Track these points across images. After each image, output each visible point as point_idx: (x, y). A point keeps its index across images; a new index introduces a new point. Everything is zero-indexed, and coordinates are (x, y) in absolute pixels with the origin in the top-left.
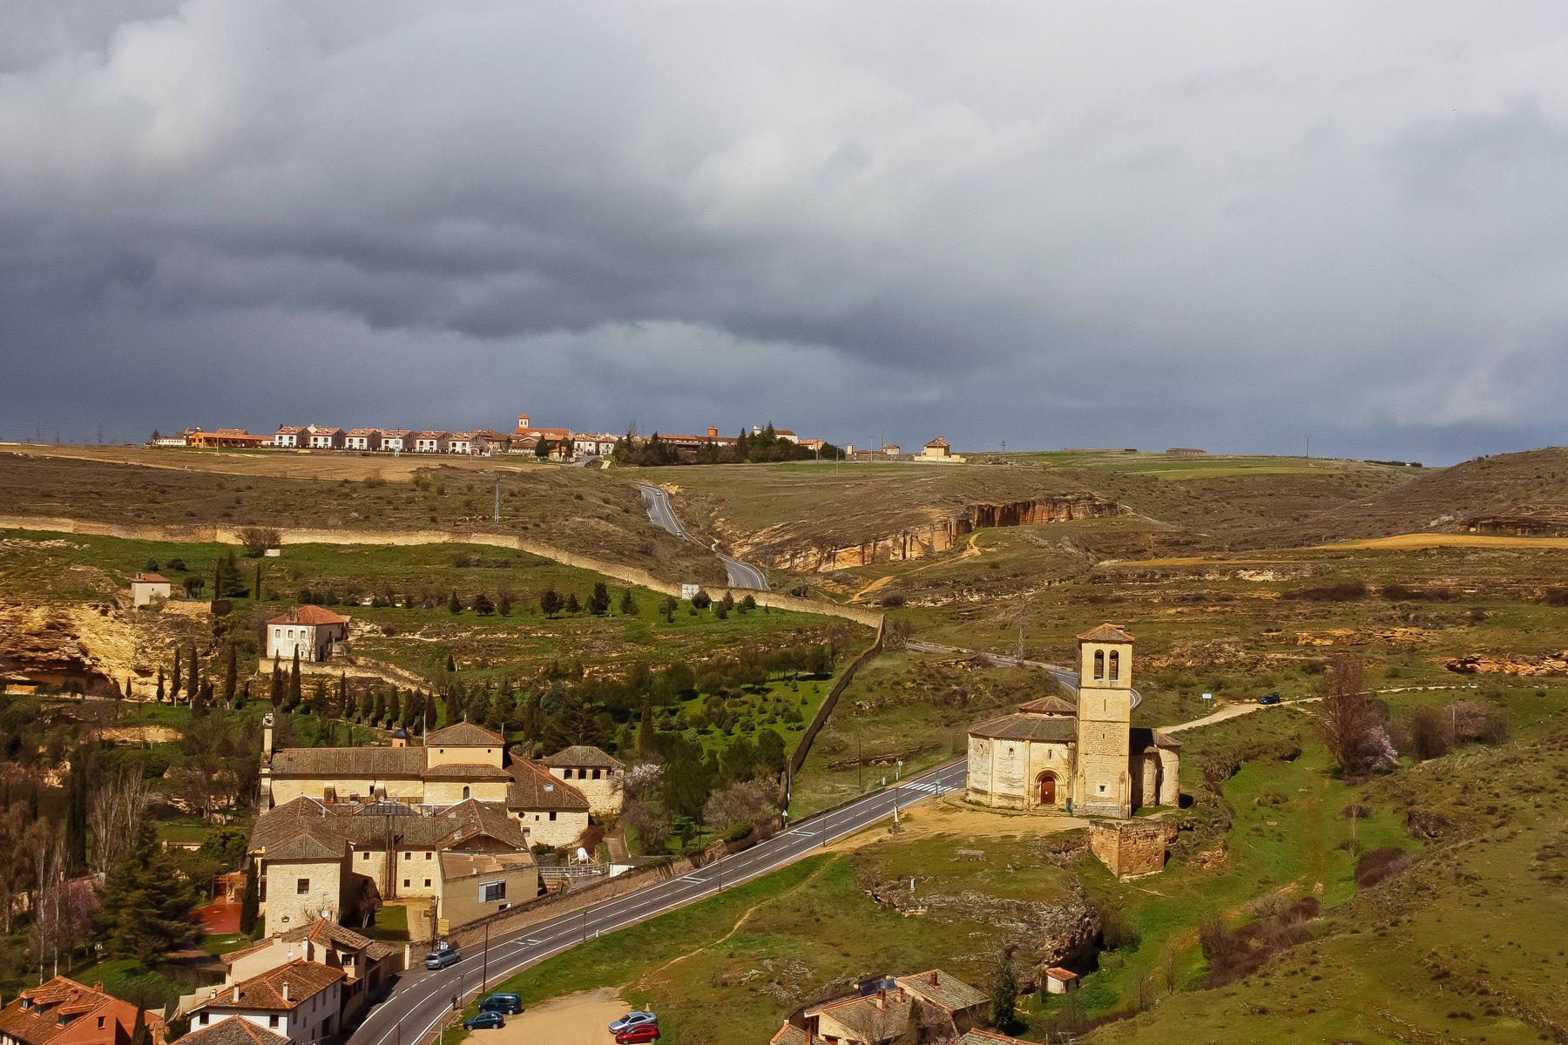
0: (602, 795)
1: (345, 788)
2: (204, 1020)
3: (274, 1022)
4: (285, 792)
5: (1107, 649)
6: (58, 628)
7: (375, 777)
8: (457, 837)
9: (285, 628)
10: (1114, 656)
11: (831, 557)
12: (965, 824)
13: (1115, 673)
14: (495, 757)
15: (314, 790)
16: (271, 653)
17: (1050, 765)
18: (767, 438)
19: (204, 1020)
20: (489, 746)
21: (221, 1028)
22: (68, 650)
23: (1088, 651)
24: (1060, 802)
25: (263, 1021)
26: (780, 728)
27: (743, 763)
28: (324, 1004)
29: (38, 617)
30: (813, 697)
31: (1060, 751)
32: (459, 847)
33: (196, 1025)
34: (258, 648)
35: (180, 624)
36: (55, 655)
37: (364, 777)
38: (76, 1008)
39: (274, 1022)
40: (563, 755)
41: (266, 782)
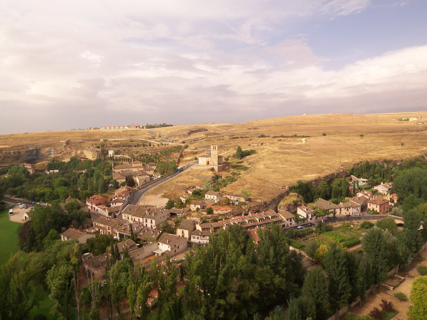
0: (154, 168)
1: (124, 170)
2: (114, 199)
3: (123, 198)
4: (116, 171)
5: (214, 146)
6: (82, 153)
7: (127, 168)
8: (139, 174)
9: (111, 151)
10: (215, 147)
11: (175, 138)
12: (199, 168)
13: (215, 149)
14: (141, 165)
15: (120, 170)
16: (109, 154)
17: (208, 160)
18: (164, 124)
19: (114, 199)
20: (141, 163)
21: (117, 199)
22: (83, 156)
23: (212, 147)
24: (210, 164)
25: (121, 198)
26: (175, 159)
27: (90, 167)
28: (172, 126)
29: (79, 152)
30: (177, 155)
31: (209, 158)
32: (139, 176)
33: (113, 199)
34: (108, 153)
35: (97, 151)
36: (82, 156)
37: (125, 168)
38: (98, 198)
39: (123, 198)
40: (149, 164)
41: (113, 170)
